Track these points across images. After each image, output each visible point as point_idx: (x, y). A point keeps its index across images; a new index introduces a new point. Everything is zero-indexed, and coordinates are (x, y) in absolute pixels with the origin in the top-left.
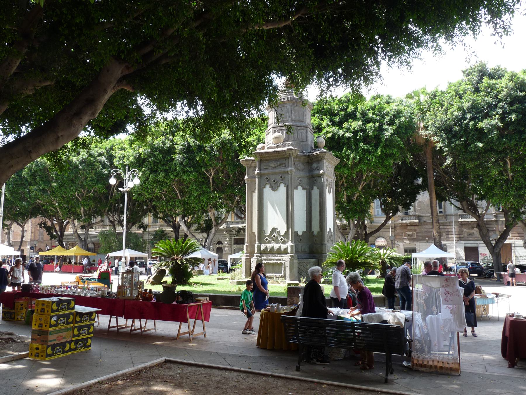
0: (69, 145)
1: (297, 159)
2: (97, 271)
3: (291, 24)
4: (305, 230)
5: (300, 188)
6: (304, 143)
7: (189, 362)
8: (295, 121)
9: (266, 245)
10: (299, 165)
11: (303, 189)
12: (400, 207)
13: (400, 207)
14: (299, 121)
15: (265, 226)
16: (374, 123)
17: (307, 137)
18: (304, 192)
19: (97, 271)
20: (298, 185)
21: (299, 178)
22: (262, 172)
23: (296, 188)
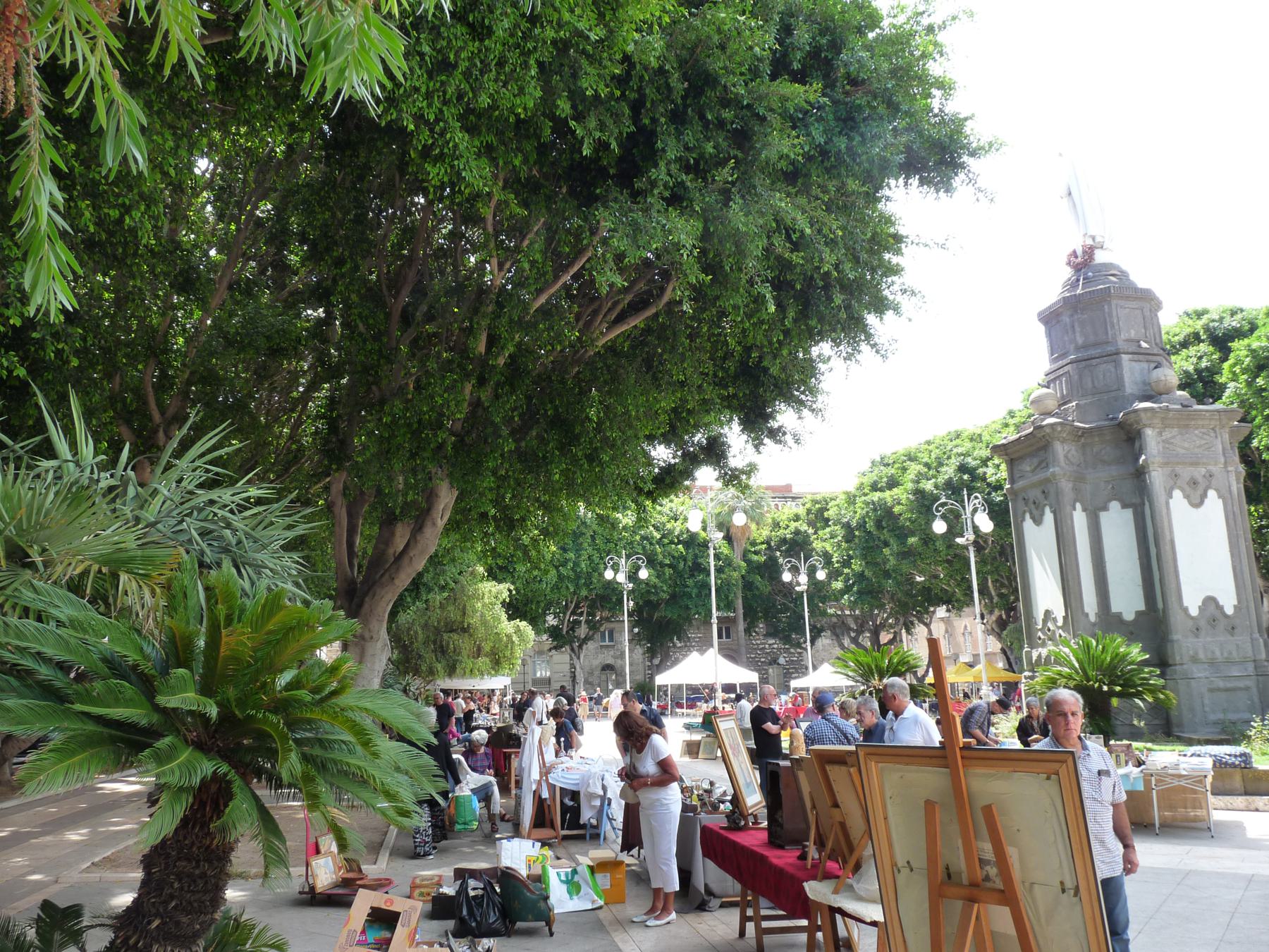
0: (863, 338)
1: (1097, 439)
2: (712, 646)
3: (720, 614)
4: (1141, 606)
5: (1115, 505)
6: (1113, 394)
7: (890, 814)
8: (1085, 347)
9: (1040, 649)
10: (1103, 452)
11: (1124, 506)
12: (213, 17)
13: (213, 17)
14: (1095, 345)
15: (1034, 608)
16: (174, 308)
17: (1120, 379)
18: (1128, 514)
19: (712, 646)
20: (1110, 500)
21: (1108, 482)
22: (1016, 486)
23: (1105, 508)
